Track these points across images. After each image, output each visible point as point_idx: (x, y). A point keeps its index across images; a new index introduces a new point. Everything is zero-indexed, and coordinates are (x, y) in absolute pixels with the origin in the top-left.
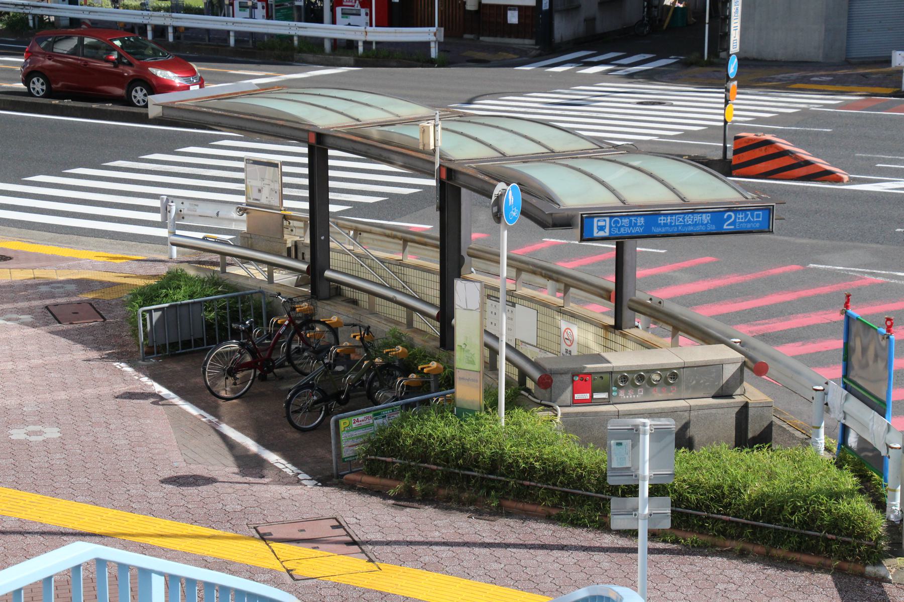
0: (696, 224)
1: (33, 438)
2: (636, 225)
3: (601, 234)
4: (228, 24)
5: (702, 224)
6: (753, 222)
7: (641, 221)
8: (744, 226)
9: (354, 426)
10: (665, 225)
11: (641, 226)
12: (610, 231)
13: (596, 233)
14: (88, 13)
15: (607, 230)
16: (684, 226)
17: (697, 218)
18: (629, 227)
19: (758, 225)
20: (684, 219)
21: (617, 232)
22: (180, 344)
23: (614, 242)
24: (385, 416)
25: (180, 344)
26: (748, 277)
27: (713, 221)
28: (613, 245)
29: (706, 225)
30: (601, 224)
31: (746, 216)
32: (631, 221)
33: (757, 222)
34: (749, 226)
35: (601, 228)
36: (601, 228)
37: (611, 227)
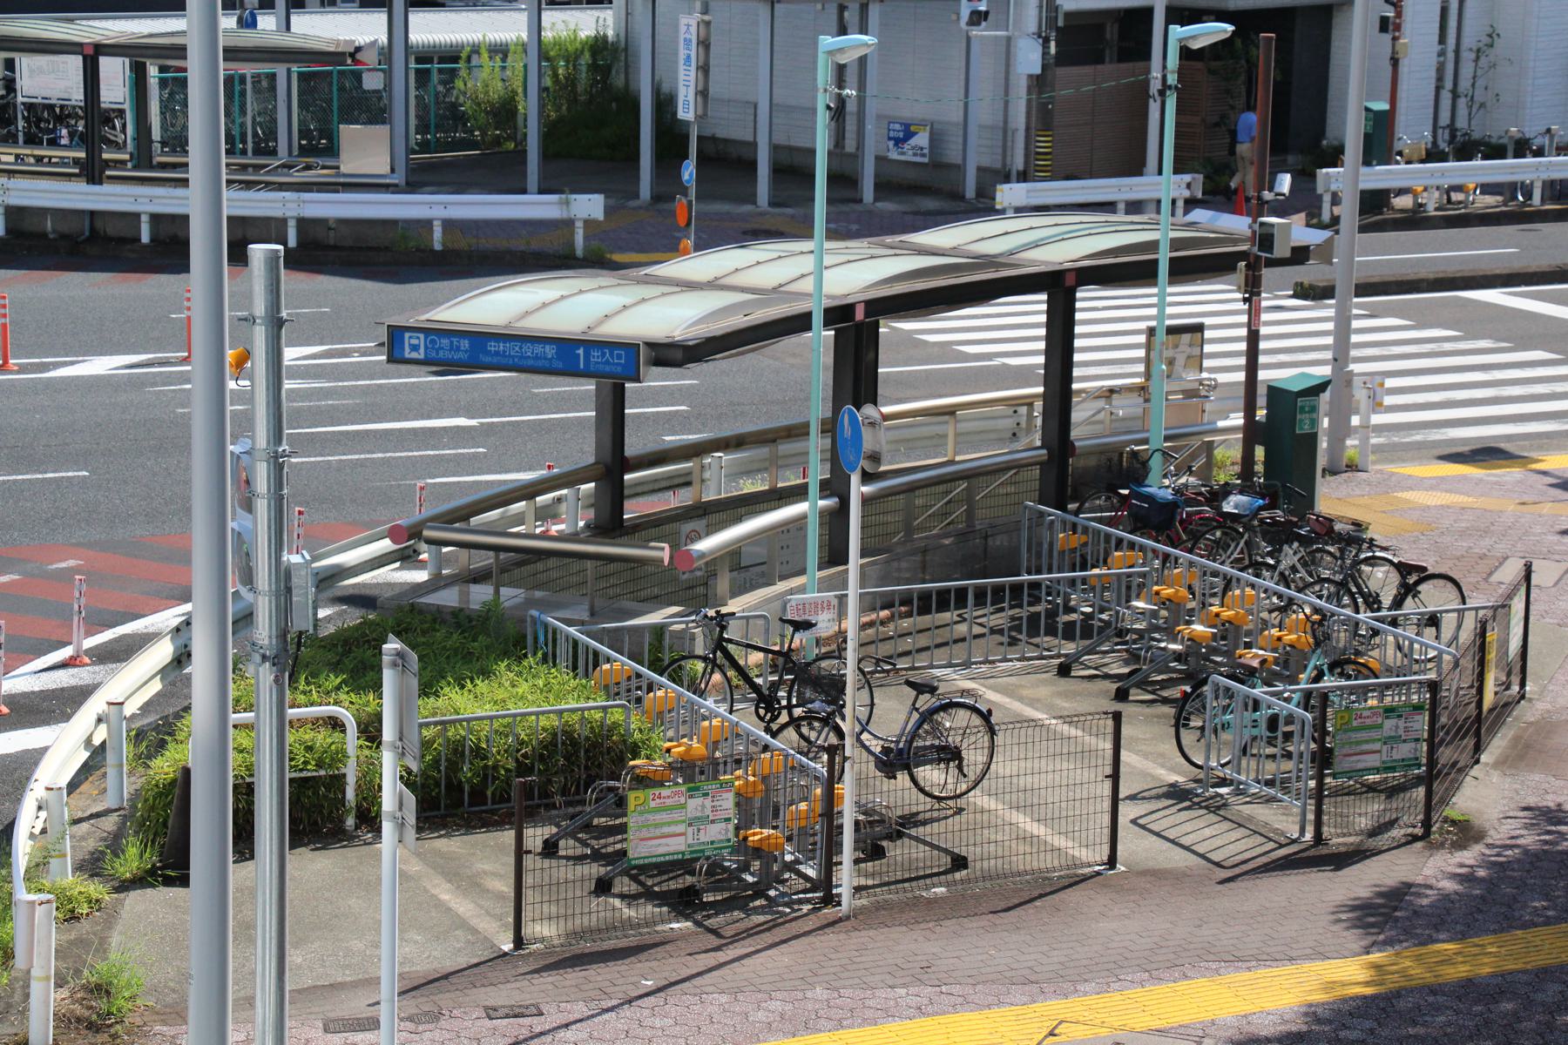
0: (537, 358)
1: (758, 830)
2: (458, 348)
3: (414, 355)
4: (155, 201)
5: (545, 359)
6: (614, 364)
7: (465, 344)
8: (601, 367)
9: (653, 804)
10: (497, 353)
11: (466, 351)
12: (426, 353)
13: (408, 354)
14: (148, 200)
15: (422, 350)
16: (521, 358)
17: (539, 349)
18: (451, 350)
19: (619, 369)
20: (521, 348)
21: (434, 355)
22: (934, 597)
23: (593, 381)
24: (707, 794)
25: (934, 597)
26: (474, 422)
27: (559, 356)
28: (1084, 447)
29: (550, 360)
30: (414, 342)
31: (603, 355)
32: (452, 342)
33: (617, 364)
34: (607, 369)
35: (415, 348)
36: (415, 348)
37: (426, 348)
